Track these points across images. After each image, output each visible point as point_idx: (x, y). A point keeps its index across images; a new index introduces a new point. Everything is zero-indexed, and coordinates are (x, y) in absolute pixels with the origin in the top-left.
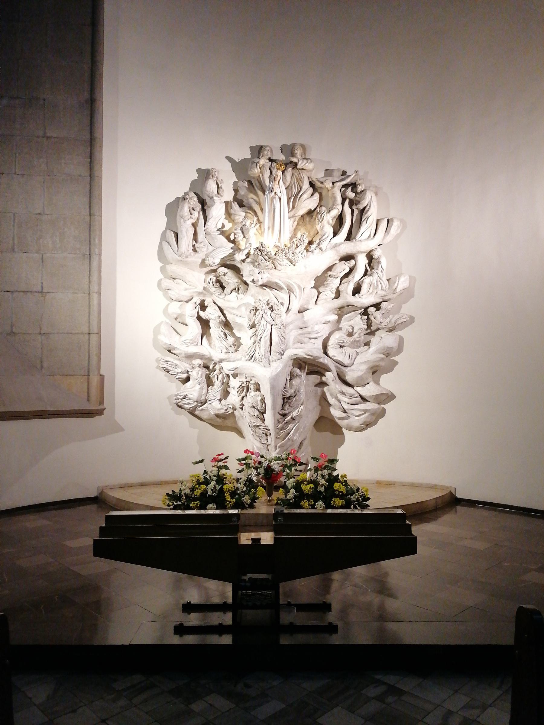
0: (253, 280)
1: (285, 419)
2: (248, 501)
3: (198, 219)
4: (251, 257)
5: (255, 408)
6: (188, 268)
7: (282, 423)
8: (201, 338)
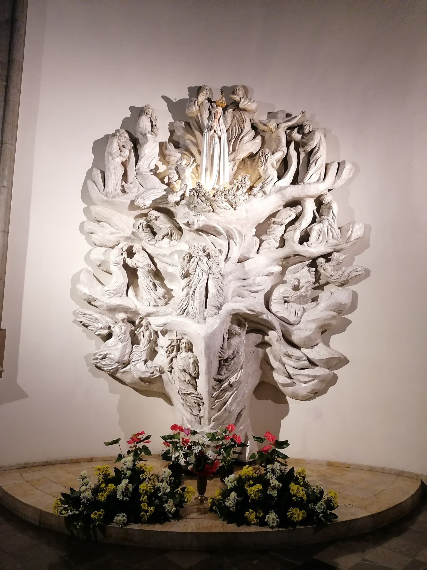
0: (188, 222)
1: (222, 385)
2: (171, 509)
3: (129, 158)
4: (186, 199)
5: (186, 372)
6: (115, 210)
7: (218, 390)
8: (126, 288)
